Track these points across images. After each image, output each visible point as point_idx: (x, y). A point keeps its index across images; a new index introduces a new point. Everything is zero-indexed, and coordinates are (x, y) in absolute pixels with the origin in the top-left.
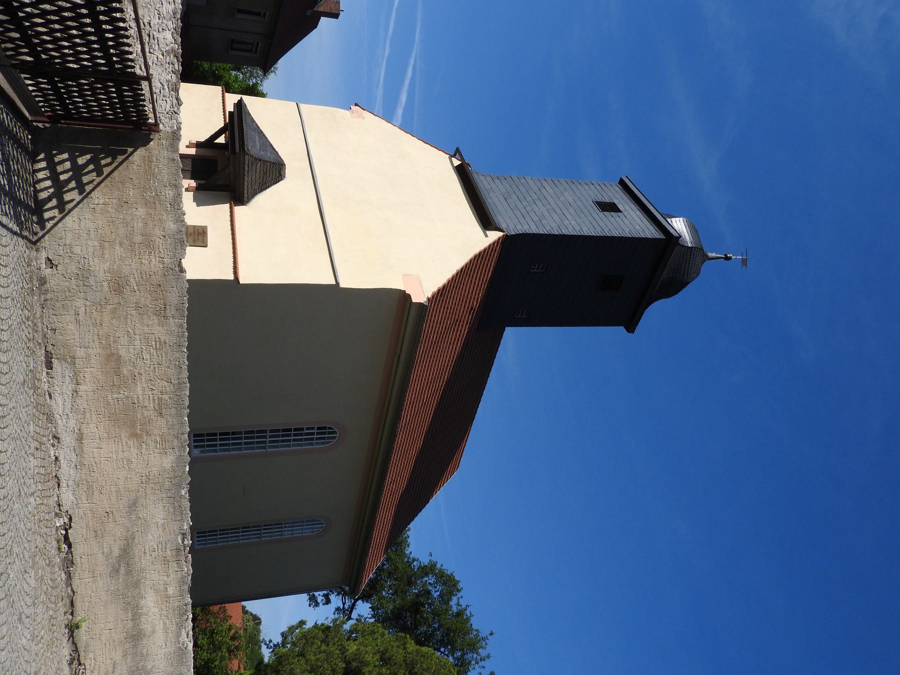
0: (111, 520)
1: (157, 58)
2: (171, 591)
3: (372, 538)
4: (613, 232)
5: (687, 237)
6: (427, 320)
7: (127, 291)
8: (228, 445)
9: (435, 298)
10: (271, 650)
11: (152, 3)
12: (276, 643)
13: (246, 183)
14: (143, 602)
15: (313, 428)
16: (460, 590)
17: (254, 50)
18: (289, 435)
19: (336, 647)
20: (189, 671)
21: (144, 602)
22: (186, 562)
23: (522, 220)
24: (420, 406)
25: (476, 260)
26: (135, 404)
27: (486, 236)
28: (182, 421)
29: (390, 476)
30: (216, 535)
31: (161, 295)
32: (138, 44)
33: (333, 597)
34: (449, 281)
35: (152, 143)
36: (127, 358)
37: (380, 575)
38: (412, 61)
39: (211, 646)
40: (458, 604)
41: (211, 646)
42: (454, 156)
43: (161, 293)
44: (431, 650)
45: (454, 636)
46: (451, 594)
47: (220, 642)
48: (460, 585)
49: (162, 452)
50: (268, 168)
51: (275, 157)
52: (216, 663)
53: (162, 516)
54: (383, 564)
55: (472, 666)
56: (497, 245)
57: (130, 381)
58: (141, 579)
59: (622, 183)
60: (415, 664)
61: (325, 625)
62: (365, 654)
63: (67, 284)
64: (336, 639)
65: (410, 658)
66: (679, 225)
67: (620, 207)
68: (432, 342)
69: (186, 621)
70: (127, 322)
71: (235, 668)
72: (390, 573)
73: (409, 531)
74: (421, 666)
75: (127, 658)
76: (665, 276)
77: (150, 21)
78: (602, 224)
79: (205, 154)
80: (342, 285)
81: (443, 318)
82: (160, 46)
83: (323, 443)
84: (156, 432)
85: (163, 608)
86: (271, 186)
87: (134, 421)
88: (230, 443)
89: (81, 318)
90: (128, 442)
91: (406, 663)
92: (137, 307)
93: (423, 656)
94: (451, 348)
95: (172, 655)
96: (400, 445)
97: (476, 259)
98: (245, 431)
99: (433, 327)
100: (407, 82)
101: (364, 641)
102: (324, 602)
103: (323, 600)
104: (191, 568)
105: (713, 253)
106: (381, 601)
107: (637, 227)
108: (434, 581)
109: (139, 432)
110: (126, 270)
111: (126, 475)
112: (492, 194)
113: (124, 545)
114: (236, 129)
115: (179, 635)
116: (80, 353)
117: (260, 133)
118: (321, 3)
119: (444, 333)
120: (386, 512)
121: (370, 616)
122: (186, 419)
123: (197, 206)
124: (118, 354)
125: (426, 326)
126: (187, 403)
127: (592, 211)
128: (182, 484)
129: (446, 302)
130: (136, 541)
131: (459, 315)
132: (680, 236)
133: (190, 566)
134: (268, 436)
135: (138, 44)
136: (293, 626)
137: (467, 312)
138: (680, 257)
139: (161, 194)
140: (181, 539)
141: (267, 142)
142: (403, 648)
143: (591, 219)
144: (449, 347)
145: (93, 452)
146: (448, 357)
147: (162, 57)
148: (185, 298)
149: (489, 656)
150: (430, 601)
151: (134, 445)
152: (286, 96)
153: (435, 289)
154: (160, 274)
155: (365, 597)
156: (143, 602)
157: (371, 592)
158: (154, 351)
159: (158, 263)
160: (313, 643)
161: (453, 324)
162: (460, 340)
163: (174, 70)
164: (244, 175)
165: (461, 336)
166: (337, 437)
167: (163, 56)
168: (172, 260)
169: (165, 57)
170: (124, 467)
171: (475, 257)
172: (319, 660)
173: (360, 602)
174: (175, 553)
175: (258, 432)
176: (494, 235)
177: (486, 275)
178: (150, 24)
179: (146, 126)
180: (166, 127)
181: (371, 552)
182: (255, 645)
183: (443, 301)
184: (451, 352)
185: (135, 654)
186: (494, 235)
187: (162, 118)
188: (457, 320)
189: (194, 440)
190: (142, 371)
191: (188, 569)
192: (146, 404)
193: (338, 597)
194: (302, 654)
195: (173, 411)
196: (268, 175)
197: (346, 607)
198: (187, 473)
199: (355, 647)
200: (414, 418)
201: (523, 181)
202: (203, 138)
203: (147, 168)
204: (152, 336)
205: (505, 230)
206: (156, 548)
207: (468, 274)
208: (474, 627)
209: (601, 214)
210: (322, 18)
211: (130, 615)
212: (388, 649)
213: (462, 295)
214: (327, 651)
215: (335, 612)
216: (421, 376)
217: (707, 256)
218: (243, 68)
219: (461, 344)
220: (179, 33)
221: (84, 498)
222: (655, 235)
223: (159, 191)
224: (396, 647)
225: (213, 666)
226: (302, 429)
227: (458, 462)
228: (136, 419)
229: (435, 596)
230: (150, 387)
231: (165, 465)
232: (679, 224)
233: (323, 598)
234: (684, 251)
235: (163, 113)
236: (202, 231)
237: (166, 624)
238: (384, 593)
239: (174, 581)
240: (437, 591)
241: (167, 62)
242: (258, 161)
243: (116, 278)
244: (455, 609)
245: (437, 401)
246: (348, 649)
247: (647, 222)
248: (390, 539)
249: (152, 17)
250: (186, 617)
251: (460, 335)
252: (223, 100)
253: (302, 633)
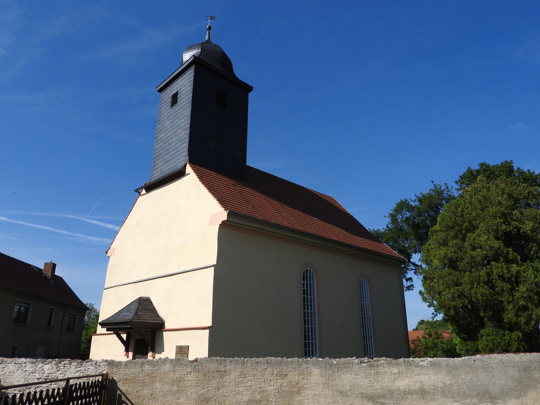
1: (61, 374)
2: (396, 371)
3: (370, 250)
4: (190, 96)
5: (197, 51)
6: (239, 211)
7: (207, 395)
8: (312, 336)
9: (225, 206)
10: (438, 313)
11: (25, 377)
12: (434, 311)
13: (151, 321)
14: (402, 388)
15: (304, 283)
16: (406, 199)
17: (75, 316)
18: (307, 298)
19: (436, 273)
20: (445, 361)
21: (402, 387)
22: (378, 361)
23: (180, 152)
24: (292, 218)
25: (204, 181)
26: (279, 391)
27: (189, 174)
28: (291, 362)
29: (335, 238)
30: (367, 344)
31: (211, 374)
32: (51, 387)
33: (408, 276)
34: (215, 197)
35: (115, 378)
36: (250, 396)
37: (396, 248)
38: (87, 220)
39: (434, 349)
40: (415, 201)
41: (434, 349)
42: (140, 193)
43: (209, 374)
44: (440, 216)
45: (433, 204)
46: (408, 205)
47: (432, 344)
48: (403, 199)
49: (310, 375)
50: (142, 307)
51: (136, 303)
52: (445, 346)
53: (350, 376)
54: (390, 245)
55: (451, 194)
57: (265, 394)
58: (387, 389)
59: (160, 91)
60: (447, 225)
61: (423, 279)
62: (440, 255)
64: (431, 272)
65: (444, 229)
66: (187, 56)
67: (175, 92)
68: (253, 209)
69: (414, 362)
70: (228, 396)
71: (448, 335)
72: (395, 241)
73: (370, 229)
74: (449, 222)
75: (436, 398)
76: (218, 66)
77: (37, 379)
78: (184, 103)
79: (133, 346)
80: (215, 263)
81: (238, 202)
82: (53, 372)
83: (313, 278)
84: (297, 378)
85: (406, 376)
86: (153, 306)
87: (290, 392)
88: (311, 335)
90: (302, 396)
91: (447, 231)
92: (218, 389)
93: (443, 220)
94: (257, 198)
95: (435, 370)
96: (316, 231)
97: (203, 180)
98: (304, 325)
99: (243, 208)
100: (100, 223)
101: (433, 256)
102: (411, 281)
103: (410, 282)
104: (382, 358)
105: (206, 37)
107: (187, 82)
108: (401, 215)
109: (297, 389)
110: (194, 396)
111: (323, 398)
112: (164, 170)
113: (366, 399)
114: (117, 327)
115: (423, 366)
117: (120, 312)
118: (46, 274)
119: (248, 202)
120: (356, 241)
121: (420, 254)
122: (289, 359)
123: (164, 352)
124: (247, 401)
125: (242, 212)
126: (279, 359)
127: (176, 109)
128: (330, 363)
129: (228, 200)
130: (364, 392)
131: (237, 192)
132: (194, 55)
133: (381, 359)
135: (51, 387)
136: (423, 298)
137: (235, 188)
138: (207, 57)
139: (147, 373)
140: (364, 364)
141: (126, 307)
142: (437, 233)
143: (181, 110)
144: (257, 199)
146: (263, 200)
147: (60, 371)
148: (214, 359)
149: (446, 184)
150: (412, 218)
151: (304, 392)
152: (100, 297)
153: (220, 206)
154: (198, 374)
155: (409, 256)
156: (402, 388)
157: (406, 253)
158: (246, 378)
159: (191, 376)
160: (433, 287)
161: (242, 196)
162: (253, 192)
163: (69, 364)
164: (145, 322)
165: (250, 191)
166: (310, 269)
167: (60, 370)
168: (189, 367)
169: (60, 369)
170: (318, 399)
171: (201, 181)
172: (443, 283)
173: (412, 260)
174: (373, 368)
175: (305, 317)
176: (189, 169)
177: (213, 175)
178: (38, 379)
179: (103, 382)
180: (105, 369)
181: (381, 251)
182: (436, 323)
183: (227, 202)
184: (260, 198)
185: (434, 394)
186: (189, 169)
187: (99, 372)
188: (240, 194)
189: (308, 356)
190: (259, 386)
191: (382, 360)
192: (279, 384)
193: (408, 273)
194: (440, 293)
195: (284, 367)
196: (146, 308)
197: (414, 268)
198: (323, 359)
199: (436, 261)
200: (302, 224)
201: (157, 151)
202: (122, 348)
203: (131, 382)
205: (186, 162)
206: (369, 379)
207: (212, 186)
208: (428, 192)
209: (179, 104)
210: (55, 274)
211: (409, 396)
212: (437, 241)
213: (222, 187)
214: (438, 278)
215: (417, 275)
216: (274, 216)
217: (207, 40)
218: (89, 324)
219: (255, 192)
220: (45, 360)
222: (193, 71)
223: (145, 374)
224: (437, 236)
225: (446, 348)
226: (304, 290)
227: (328, 197)
228: (288, 391)
229: (409, 215)
230: (268, 381)
231: (318, 373)
232: (187, 57)
233: (408, 282)
234: (204, 54)
235: (96, 371)
236: (179, 349)
237: (416, 374)
238: (407, 245)
239: (390, 369)
240: (406, 214)
241: (63, 368)
242: (137, 314)
243: (199, 402)
244: (417, 203)
245: (290, 208)
246: (437, 266)
247: (184, 75)
248: (369, 239)
249: (34, 377)
250: (412, 361)
251: (250, 192)
252: (100, 335)
253: (427, 293)
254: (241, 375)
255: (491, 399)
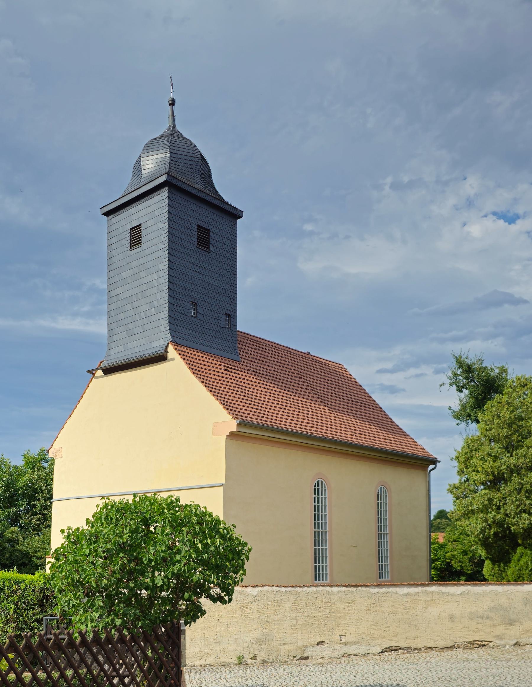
0: (388, 629)
15: (315, 498)
27: (173, 359)
56: (180, 350)
63: (265, 649)
89: (282, 643)
106: (462, 518)
116: (300, 643)
134: (319, 530)
145: (353, 637)
176: (172, 352)
186: (172, 352)
190: (310, 612)
192: (328, 610)
204: (291, 607)
205: (167, 342)
209: (144, 246)
221: (376, 642)
226: (315, 506)
230: (318, 608)
254: (295, 603)
255: (480, 417)
